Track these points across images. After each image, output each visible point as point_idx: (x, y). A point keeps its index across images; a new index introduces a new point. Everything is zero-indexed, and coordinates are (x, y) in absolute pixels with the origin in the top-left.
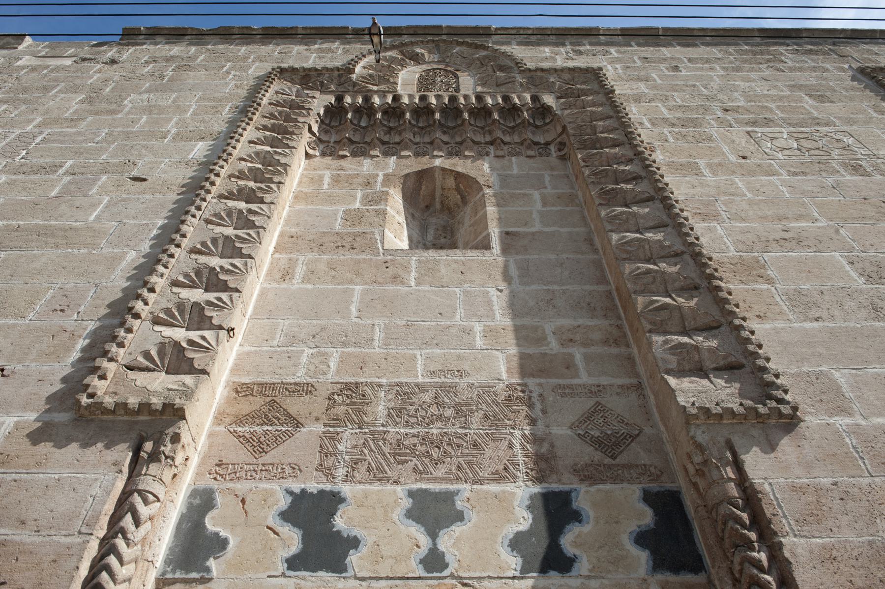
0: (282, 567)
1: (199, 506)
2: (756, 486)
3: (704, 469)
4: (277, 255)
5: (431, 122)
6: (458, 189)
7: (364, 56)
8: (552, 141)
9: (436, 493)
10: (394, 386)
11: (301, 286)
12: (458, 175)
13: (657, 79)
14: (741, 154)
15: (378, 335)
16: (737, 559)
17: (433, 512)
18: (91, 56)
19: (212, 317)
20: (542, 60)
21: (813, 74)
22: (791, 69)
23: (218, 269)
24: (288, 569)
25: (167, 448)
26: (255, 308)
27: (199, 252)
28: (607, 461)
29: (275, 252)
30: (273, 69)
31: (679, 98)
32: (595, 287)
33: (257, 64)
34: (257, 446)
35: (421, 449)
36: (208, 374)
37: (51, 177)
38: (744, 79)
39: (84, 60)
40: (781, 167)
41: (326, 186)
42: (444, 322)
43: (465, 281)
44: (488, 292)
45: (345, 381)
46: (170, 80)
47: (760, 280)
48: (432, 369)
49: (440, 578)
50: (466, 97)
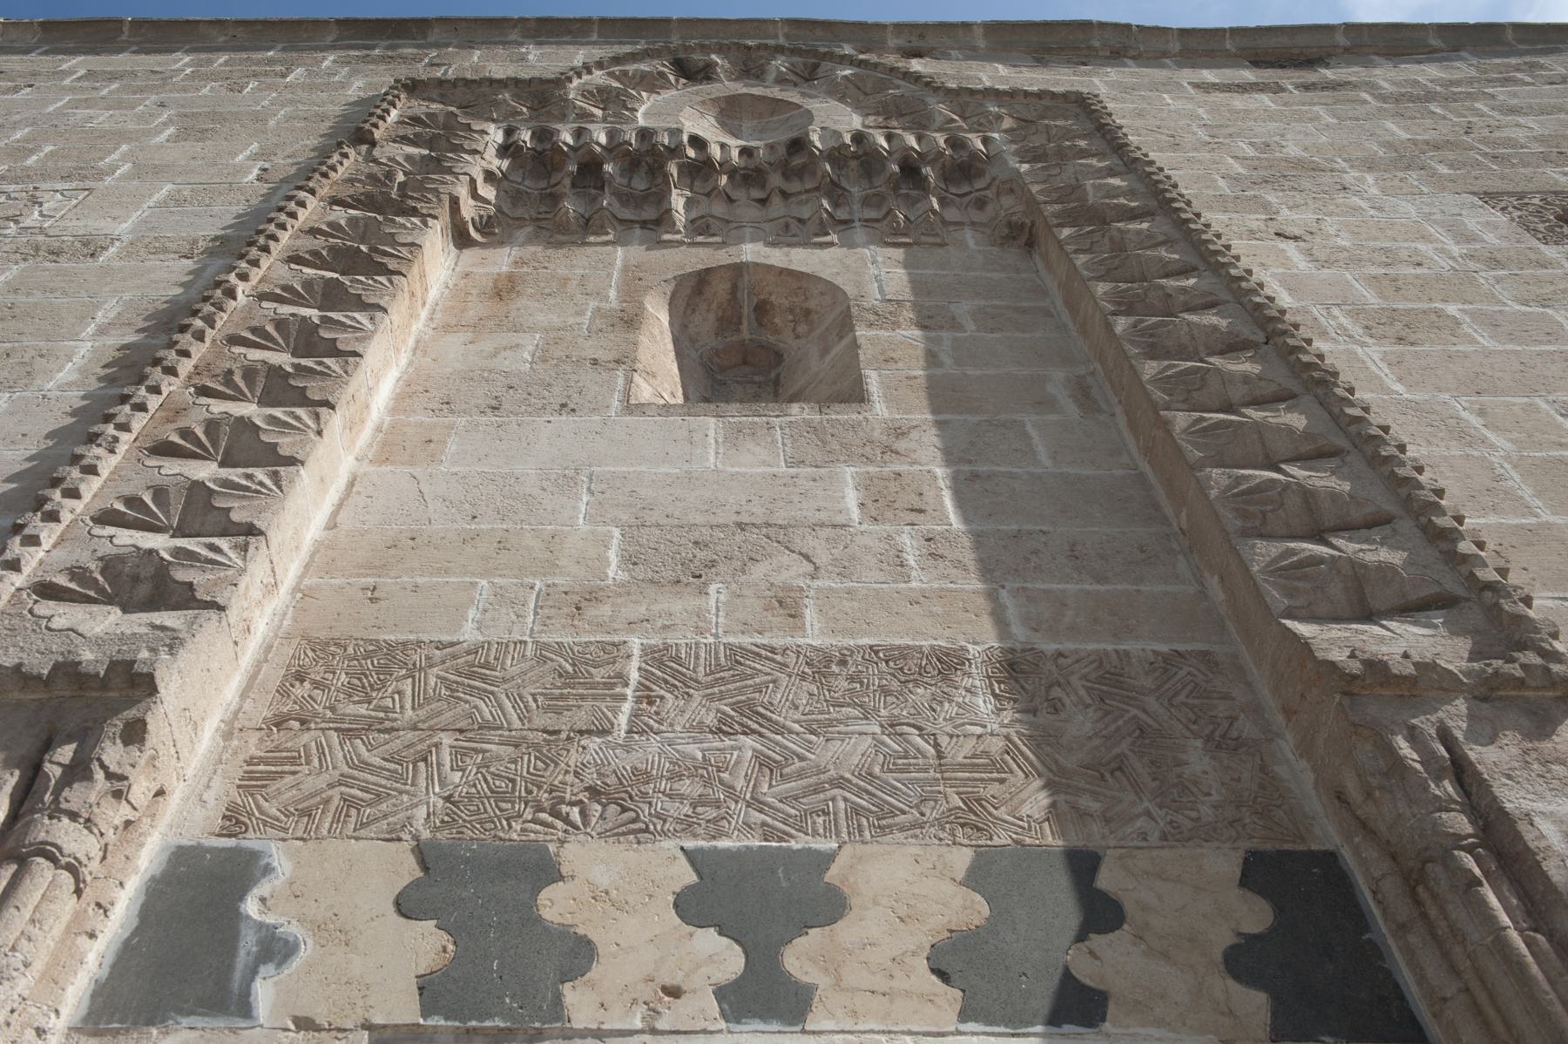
19: (229, 510)
25: (112, 753)
36: (385, 311)
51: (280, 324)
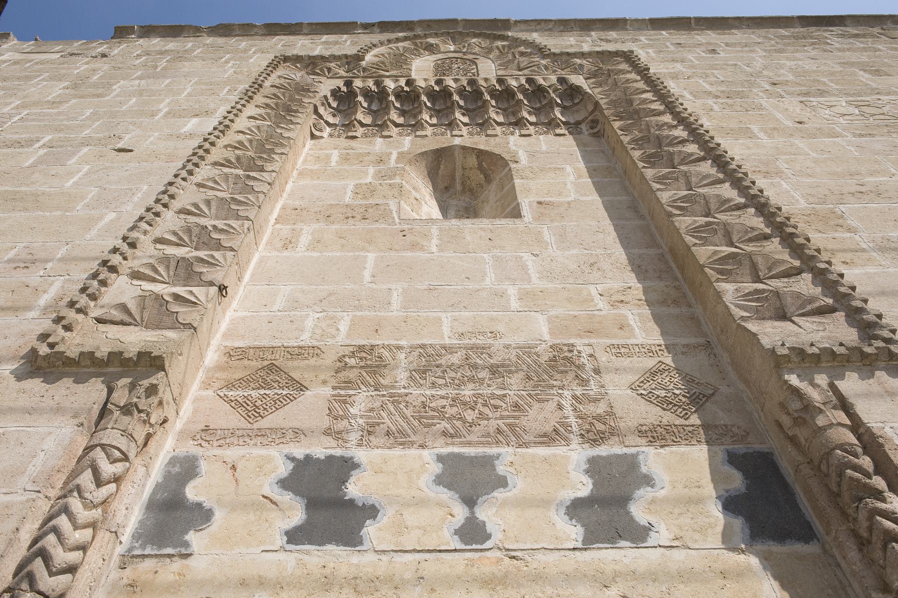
0: (280, 540)
1: (179, 474)
2: (874, 431)
3: (804, 416)
4: (278, 226)
5: (449, 104)
6: (480, 168)
7: (375, 46)
8: (583, 121)
9: (472, 458)
10: (416, 348)
11: (306, 254)
12: (481, 154)
13: (694, 60)
14: (797, 120)
15: (396, 300)
16: (862, 516)
17: (470, 480)
18: (79, 52)
19: (201, 273)
20: (566, 47)
21: (864, 53)
22: (839, 50)
23: (210, 228)
24: (288, 542)
26: (253, 275)
27: (189, 213)
28: (679, 421)
29: (276, 223)
30: (276, 57)
31: (720, 75)
32: (645, 251)
33: (259, 55)
34: (252, 411)
35: (451, 411)
37: (26, 149)
38: (788, 59)
39: (72, 54)
40: (844, 130)
41: (333, 164)
42: (471, 286)
43: (494, 247)
44: (521, 258)
45: (358, 344)
46: (163, 69)
47: (840, 229)
48: (460, 331)
49: (481, 550)
50: (486, 80)
51: (238, 158)
